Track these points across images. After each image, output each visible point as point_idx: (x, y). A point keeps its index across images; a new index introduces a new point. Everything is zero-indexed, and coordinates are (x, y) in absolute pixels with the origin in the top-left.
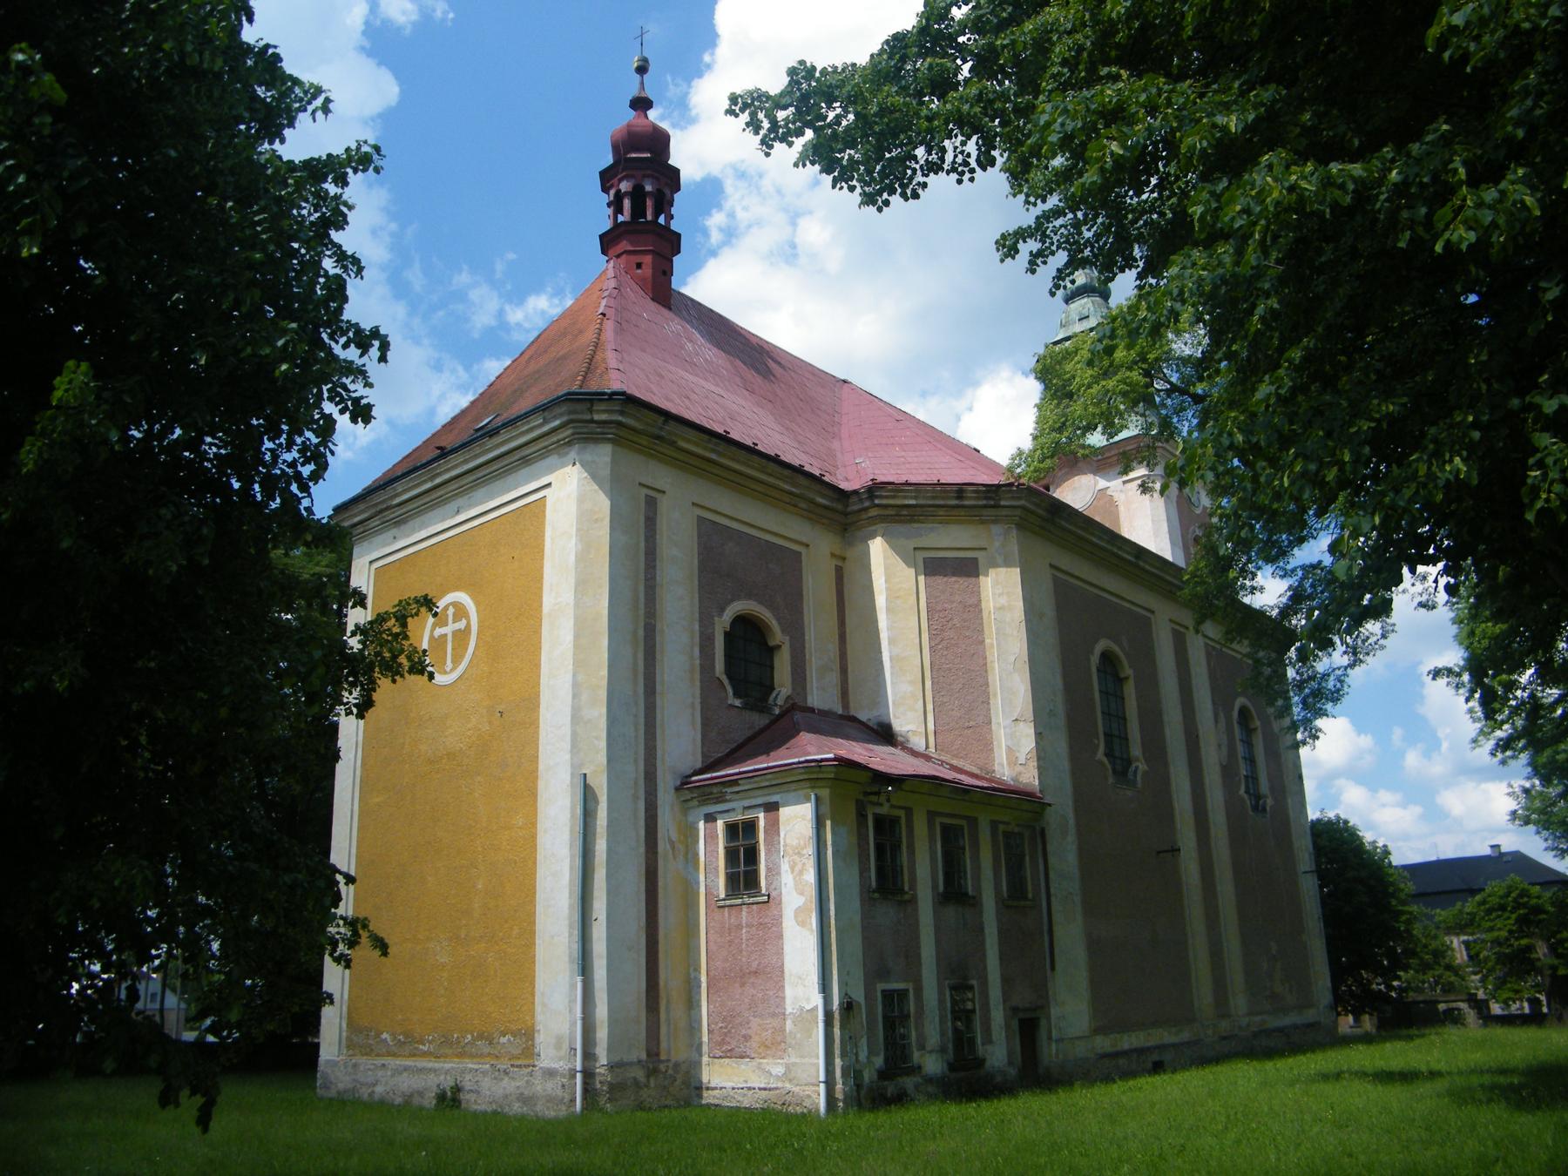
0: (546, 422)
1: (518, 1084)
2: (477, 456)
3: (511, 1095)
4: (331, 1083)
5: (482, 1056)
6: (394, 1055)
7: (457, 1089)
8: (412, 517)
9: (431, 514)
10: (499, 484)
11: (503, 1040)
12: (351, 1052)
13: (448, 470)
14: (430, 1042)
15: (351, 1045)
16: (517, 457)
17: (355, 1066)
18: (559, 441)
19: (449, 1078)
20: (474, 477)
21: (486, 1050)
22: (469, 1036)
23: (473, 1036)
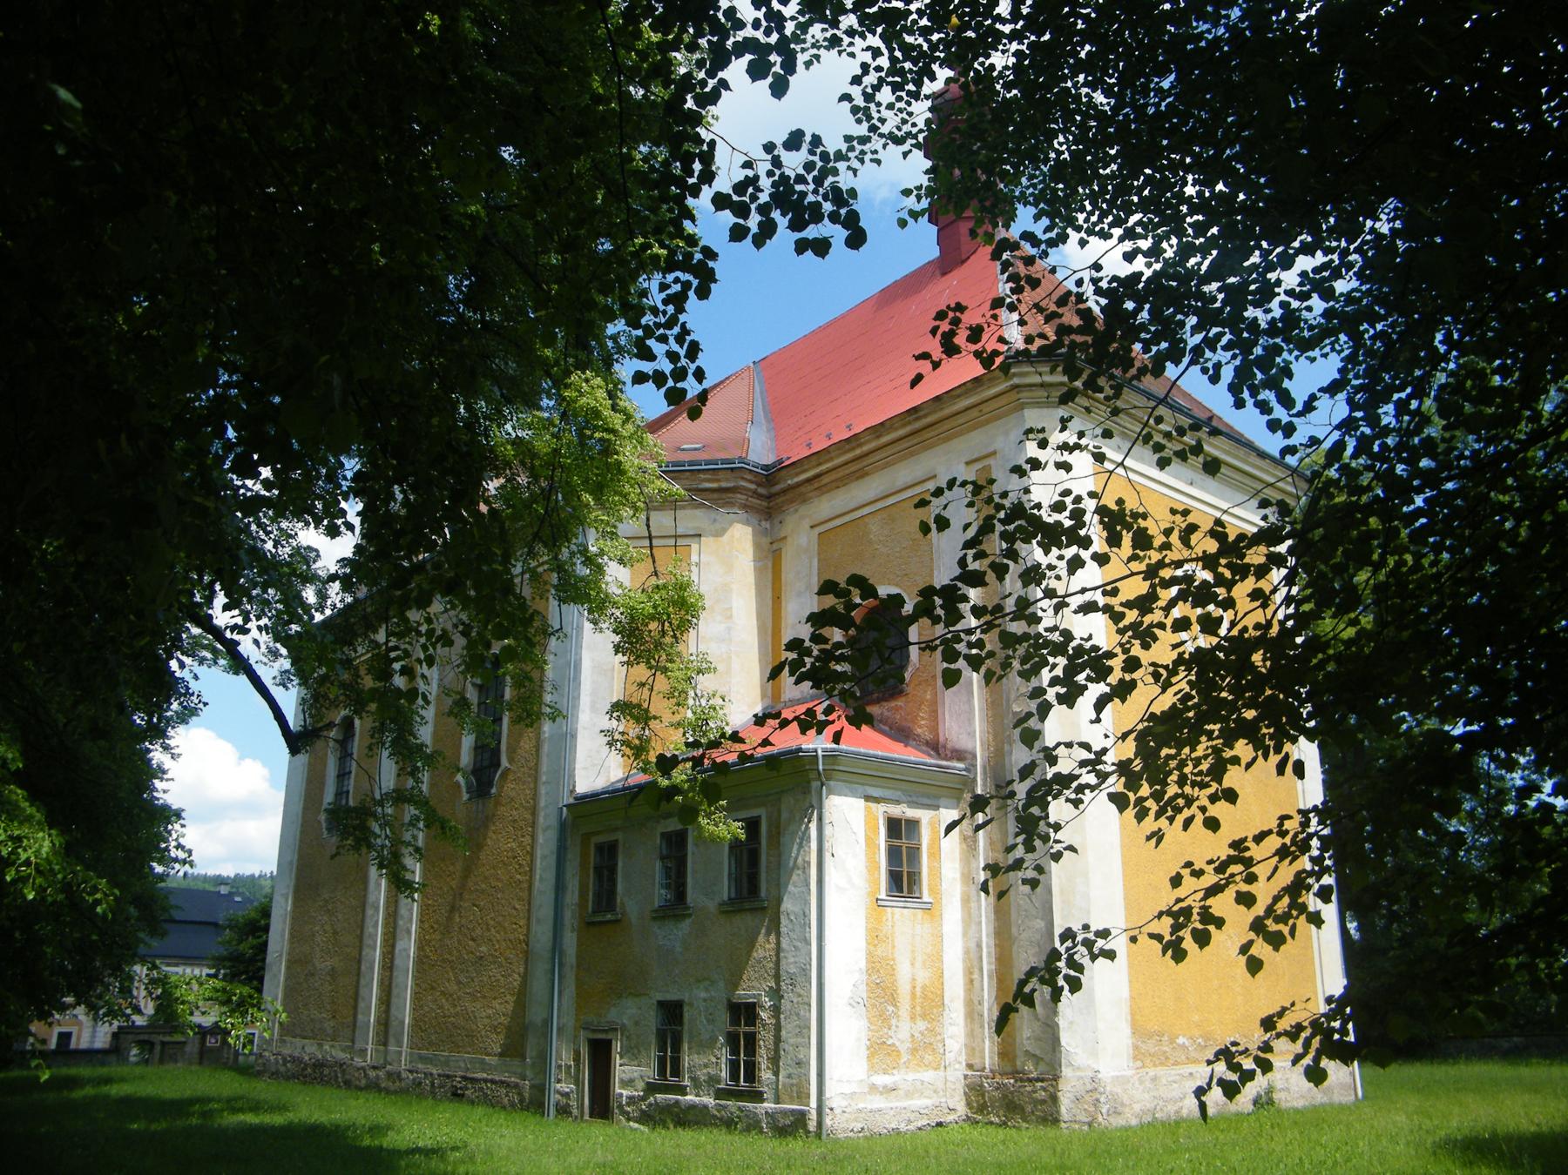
2: (1236, 457)
4: (1123, 1104)
15: (1138, 1054)
17: (1154, 1079)
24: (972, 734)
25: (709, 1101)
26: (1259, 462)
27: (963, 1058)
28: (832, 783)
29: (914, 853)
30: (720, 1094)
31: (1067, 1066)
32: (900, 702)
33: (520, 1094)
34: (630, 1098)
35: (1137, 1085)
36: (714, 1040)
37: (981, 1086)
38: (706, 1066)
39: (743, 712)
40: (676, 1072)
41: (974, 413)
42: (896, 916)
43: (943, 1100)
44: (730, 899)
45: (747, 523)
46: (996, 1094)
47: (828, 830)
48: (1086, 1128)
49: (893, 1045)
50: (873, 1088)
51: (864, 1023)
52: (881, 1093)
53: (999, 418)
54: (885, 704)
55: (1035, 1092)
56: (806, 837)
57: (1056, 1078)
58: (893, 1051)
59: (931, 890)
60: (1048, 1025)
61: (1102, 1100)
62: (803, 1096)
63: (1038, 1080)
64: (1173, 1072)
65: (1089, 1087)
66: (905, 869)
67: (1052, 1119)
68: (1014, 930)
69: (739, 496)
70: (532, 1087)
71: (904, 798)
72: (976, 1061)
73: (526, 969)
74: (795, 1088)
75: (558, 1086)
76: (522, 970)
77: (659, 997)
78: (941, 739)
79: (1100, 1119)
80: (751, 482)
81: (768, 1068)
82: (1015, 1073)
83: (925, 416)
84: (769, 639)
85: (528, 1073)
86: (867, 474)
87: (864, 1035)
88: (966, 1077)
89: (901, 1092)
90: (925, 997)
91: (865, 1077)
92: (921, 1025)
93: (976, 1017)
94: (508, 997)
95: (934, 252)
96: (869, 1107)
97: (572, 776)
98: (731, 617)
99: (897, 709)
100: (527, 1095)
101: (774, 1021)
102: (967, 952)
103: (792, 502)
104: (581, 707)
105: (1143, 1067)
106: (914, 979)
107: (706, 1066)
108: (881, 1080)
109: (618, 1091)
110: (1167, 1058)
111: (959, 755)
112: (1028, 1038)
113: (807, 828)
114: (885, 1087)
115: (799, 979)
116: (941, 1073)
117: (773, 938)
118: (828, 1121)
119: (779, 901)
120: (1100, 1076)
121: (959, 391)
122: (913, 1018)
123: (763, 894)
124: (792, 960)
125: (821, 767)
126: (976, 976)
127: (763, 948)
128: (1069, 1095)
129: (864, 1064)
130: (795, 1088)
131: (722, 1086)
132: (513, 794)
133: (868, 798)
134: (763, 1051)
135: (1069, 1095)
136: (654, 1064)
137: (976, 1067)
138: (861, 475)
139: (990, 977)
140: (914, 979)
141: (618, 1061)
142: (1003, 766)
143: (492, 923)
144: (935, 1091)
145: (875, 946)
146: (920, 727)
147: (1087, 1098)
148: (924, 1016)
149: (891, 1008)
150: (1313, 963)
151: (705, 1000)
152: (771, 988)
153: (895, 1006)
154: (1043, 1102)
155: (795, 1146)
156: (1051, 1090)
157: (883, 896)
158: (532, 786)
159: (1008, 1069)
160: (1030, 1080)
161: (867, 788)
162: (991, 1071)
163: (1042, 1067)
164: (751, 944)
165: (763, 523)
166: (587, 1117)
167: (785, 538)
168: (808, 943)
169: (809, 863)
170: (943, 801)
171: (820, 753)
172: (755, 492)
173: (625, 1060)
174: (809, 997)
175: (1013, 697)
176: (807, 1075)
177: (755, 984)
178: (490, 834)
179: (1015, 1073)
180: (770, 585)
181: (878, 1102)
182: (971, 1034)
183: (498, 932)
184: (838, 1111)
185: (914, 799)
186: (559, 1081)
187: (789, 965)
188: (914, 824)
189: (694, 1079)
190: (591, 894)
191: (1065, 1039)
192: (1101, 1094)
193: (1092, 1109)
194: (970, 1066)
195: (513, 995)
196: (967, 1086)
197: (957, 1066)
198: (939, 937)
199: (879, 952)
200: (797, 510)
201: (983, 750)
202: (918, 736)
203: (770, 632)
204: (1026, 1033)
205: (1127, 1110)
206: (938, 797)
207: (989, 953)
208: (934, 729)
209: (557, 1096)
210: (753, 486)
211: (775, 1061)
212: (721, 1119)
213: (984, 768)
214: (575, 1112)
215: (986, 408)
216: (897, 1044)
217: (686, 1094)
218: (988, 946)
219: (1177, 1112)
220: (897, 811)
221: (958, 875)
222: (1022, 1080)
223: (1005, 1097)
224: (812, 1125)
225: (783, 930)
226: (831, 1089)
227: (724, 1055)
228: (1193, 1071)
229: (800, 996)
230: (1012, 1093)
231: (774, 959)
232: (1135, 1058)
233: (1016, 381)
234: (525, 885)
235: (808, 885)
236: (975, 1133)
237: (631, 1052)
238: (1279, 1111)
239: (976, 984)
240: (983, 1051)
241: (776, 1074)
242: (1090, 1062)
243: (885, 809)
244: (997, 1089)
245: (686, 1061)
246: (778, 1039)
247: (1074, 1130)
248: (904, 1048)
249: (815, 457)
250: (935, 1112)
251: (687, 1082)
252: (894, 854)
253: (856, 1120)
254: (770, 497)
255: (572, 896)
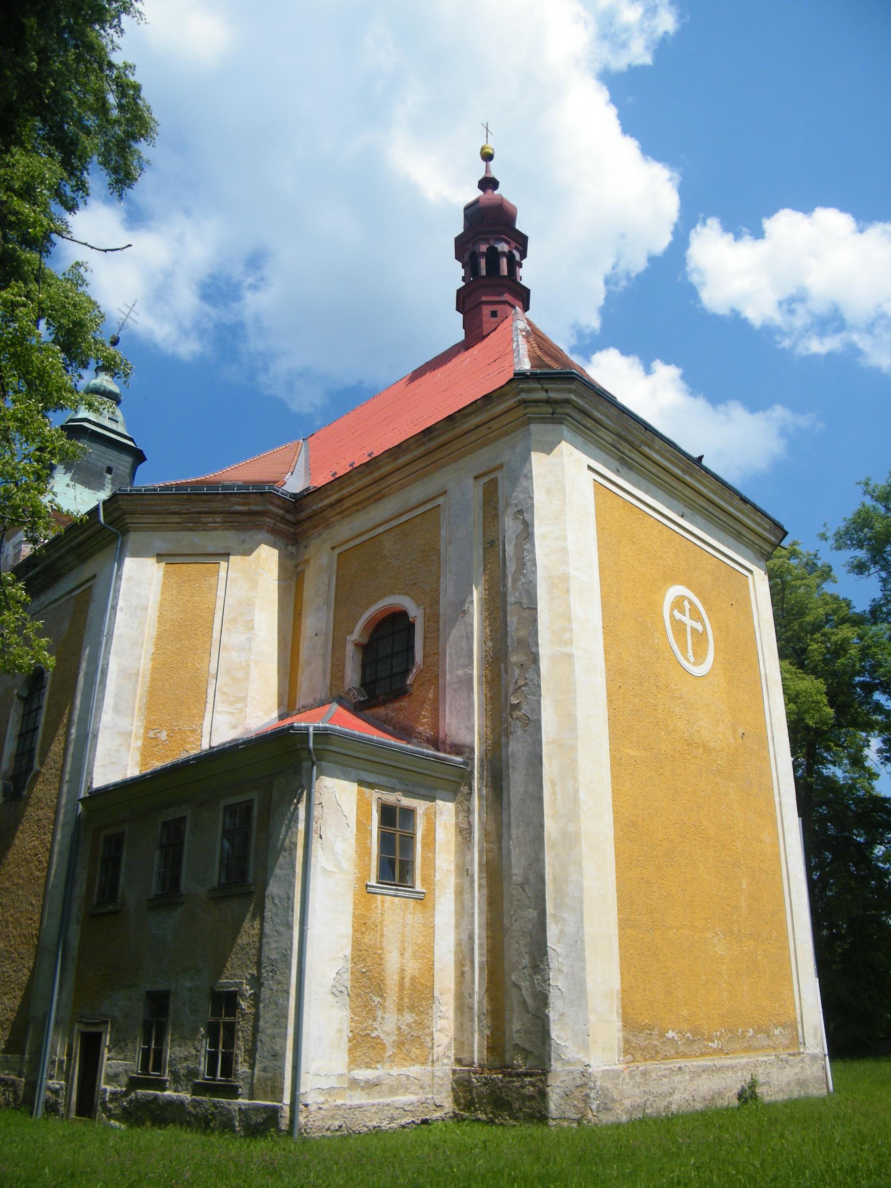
0: (769, 531)
1: (796, 1071)
2: (722, 498)
3: (792, 1081)
4: (613, 1100)
5: (763, 1048)
6: (684, 1056)
7: (753, 1084)
8: (639, 472)
9: (660, 492)
10: (715, 530)
11: (777, 1032)
12: (629, 1057)
13: (699, 481)
14: (719, 1038)
15: (628, 1048)
16: (736, 528)
17: (644, 1074)
18: (761, 548)
19: (745, 1073)
20: (706, 506)
21: (765, 1043)
22: (751, 1030)
23: (754, 1030)
24: (471, 729)
25: (186, 1096)
26: (741, 504)
27: (452, 1053)
28: (323, 764)
29: (408, 842)
30: (198, 1089)
31: (557, 1060)
32: (404, 703)
33: (15, 1092)
34: (113, 1094)
35: (627, 1080)
36: (196, 1030)
37: (469, 1081)
38: (186, 1059)
39: (258, 717)
40: (158, 1066)
41: (484, 430)
42: (386, 905)
43: (430, 1096)
44: (220, 885)
45: (274, 545)
46: (484, 1089)
47: (316, 812)
48: (575, 1125)
49: (378, 1037)
50: (354, 1083)
51: (346, 1013)
52: (363, 1089)
53: (507, 434)
54: (389, 705)
55: (523, 1087)
56: (294, 819)
57: (545, 1072)
58: (377, 1045)
59: (424, 881)
60: (538, 1017)
61: (592, 1095)
62: (276, 1092)
63: (526, 1075)
64: (663, 1066)
65: (579, 1082)
66: (398, 857)
67: (541, 1117)
68: (506, 921)
69: (267, 519)
70: (26, 1084)
71: (399, 786)
72: (465, 1056)
73: (35, 963)
74: (269, 1083)
75: (50, 1082)
76: (31, 964)
77: (149, 987)
78: (441, 735)
79: (590, 1116)
80: (279, 507)
81: (245, 1061)
82: (504, 1068)
83: (439, 436)
84: (289, 652)
85: (25, 1069)
86: (384, 496)
87: (346, 1026)
88: (454, 1072)
89: (385, 1088)
90: (414, 989)
91: (344, 1070)
92: (409, 1017)
93: (466, 1010)
94: (17, 992)
95: (459, 335)
96: (349, 1103)
97: (90, 773)
98: (252, 628)
99: (401, 709)
100: (21, 1093)
101: (253, 1010)
102: (459, 944)
103: (316, 527)
104: (105, 708)
105: (633, 1061)
106: (403, 970)
107: (186, 1059)
108: (363, 1074)
109: (103, 1086)
110: (657, 1052)
111: (458, 749)
112: (518, 1031)
113: (296, 809)
114: (367, 1082)
115: (279, 965)
116: (429, 1068)
117: (257, 923)
118: (301, 1119)
119: (265, 884)
120: (590, 1070)
121: (470, 409)
122: (400, 1010)
123: (250, 879)
124: (274, 945)
125: (311, 745)
126: (467, 968)
127: (249, 931)
128: (557, 1090)
129: (345, 1057)
130: (269, 1083)
131: (200, 1080)
132: (40, 795)
133: (362, 783)
134: (241, 1043)
135: (557, 1090)
136: (139, 1057)
137: (464, 1062)
138: (378, 497)
139: (481, 969)
140: (403, 970)
141: (106, 1054)
142: (500, 758)
143: (11, 919)
144: (421, 1087)
145: (363, 933)
146: (422, 725)
147: (577, 1093)
148: (412, 1008)
149: (377, 999)
150: (790, 963)
151: (190, 990)
152: (252, 975)
153: (382, 996)
154: (531, 1098)
155: (260, 1147)
156: (540, 1084)
157: (373, 882)
158: (57, 786)
159: (498, 1064)
160: (518, 1075)
161: (361, 772)
162: (480, 1066)
163: (531, 1061)
164: (236, 930)
165: (290, 548)
166: (73, 1115)
167: (308, 560)
168: (290, 927)
169: (295, 844)
170: (439, 793)
171: (311, 730)
172: (282, 518)
173: (112, 1054)
174: (288, 984)
175: (511, 690)
176: (282, 1068)
177: (238, 972)
178: (18, 834)
179: (504, 1068)
180: (293, 605)
181: (358, 1098)
182: (460, 1028)
183: (15, 928)
184: (312, 1108)
185: (411, 788)
186: (51, 1077)
187: (271, 952)
188: (409, 814)
189: (174, 1073)
190: (97, 885)
191: (555, 1032)
192: (591, 1088)
193: (582, 1105)
194: (459, 1061)
195: (21, 990)
196: (455, 1081)
197: (446, 1061)
198: (430, 929)
199: (366, 940)
200: (320, 535)
201: (480, 744)
202: (420, 733)
203: (290, 647)
204: (516, 1025)
205: (617, 1106)
206: (435, 789)
207: (481, 945)
208: (435, 726)
209: (48, 1093)
210: (281, 512)
211: (251, 1053)
212: (196, 1116)
213: (481, 761)
214: (62, 1109)
215: (495, 425)
216: (382, 1036)
217: (164, 1089)
218: (479, 939)
219: (667, 1108)
220: (391, 798)
221: (452, 867)
222: (510, 1075)
223: (493, 1092)
224: (284, 1123)
225: (268, 914)
226: (307, 1084)
227: (204, 1046)
228: (682, 1065)
229: (279, 983)
230: (499, 1088)
231: (257, 944)
232: (626, 1052)
233: (524, 396)
234: (42, 881)
235: (293, 867)
236: (458, 1133)
237: (118, 1044)
238: (305, 1141)
239: (467, 976)
240: (472, 1045)
241: (252, 1067)
242: (580, 1056)
243: (379, 795)
244: (485, 1084)
245: (168, 1054)
246: (256, 1029)
247: (561, 1128)
248: (388, 1040)
249: (337, 482)
250: (421, 1109)
251: (167, 1077)
252: (386, 841)
253: (333, 1118)
254: (296, 524)
255: (80, 890)
